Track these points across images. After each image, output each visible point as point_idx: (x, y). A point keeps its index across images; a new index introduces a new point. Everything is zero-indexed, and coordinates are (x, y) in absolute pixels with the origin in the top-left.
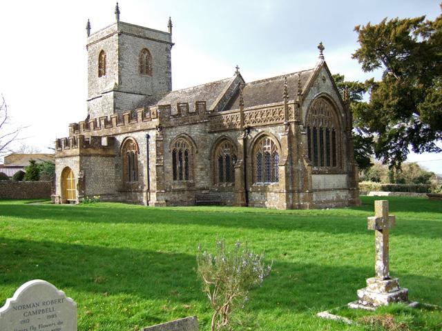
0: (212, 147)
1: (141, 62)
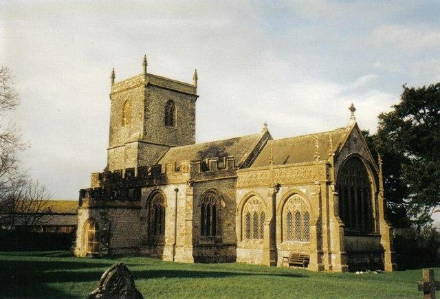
1: (166, 114)
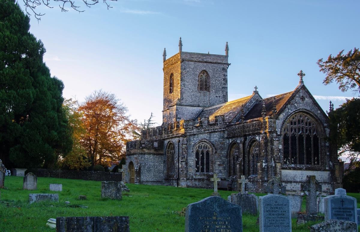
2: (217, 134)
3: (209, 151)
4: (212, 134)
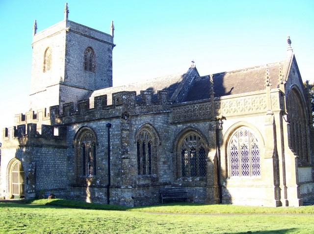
0: (175, 140)
1: (85, 59)
2: (161, 116)
3: (152, 142)
4: (157, 116)
